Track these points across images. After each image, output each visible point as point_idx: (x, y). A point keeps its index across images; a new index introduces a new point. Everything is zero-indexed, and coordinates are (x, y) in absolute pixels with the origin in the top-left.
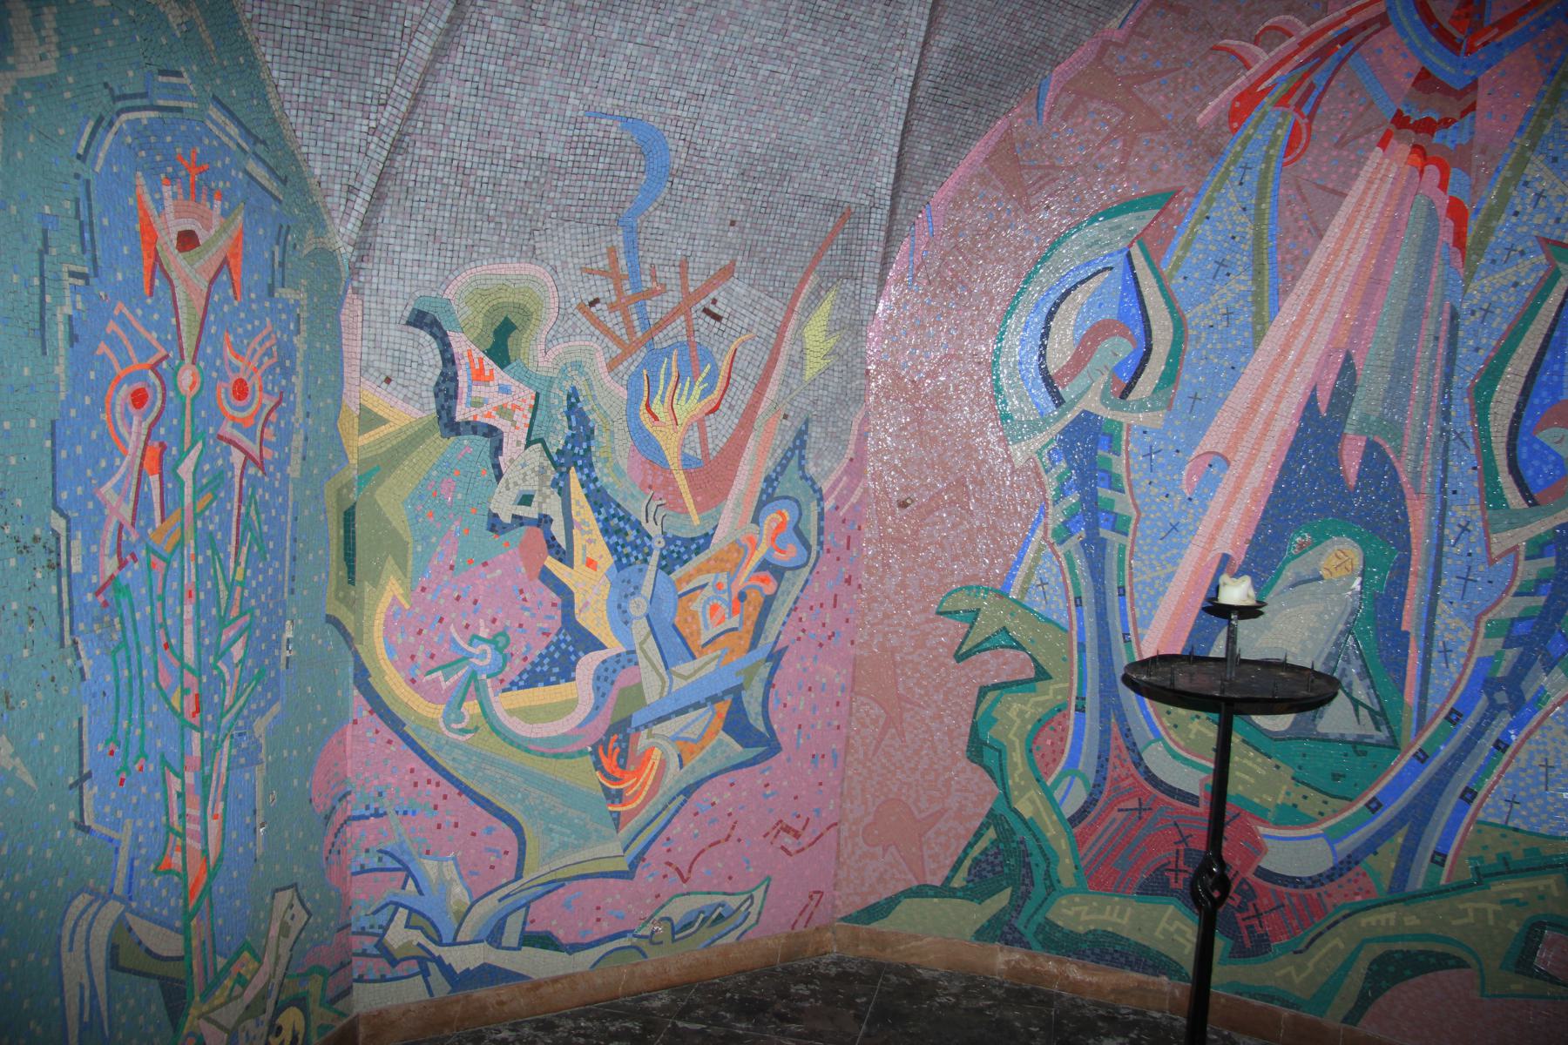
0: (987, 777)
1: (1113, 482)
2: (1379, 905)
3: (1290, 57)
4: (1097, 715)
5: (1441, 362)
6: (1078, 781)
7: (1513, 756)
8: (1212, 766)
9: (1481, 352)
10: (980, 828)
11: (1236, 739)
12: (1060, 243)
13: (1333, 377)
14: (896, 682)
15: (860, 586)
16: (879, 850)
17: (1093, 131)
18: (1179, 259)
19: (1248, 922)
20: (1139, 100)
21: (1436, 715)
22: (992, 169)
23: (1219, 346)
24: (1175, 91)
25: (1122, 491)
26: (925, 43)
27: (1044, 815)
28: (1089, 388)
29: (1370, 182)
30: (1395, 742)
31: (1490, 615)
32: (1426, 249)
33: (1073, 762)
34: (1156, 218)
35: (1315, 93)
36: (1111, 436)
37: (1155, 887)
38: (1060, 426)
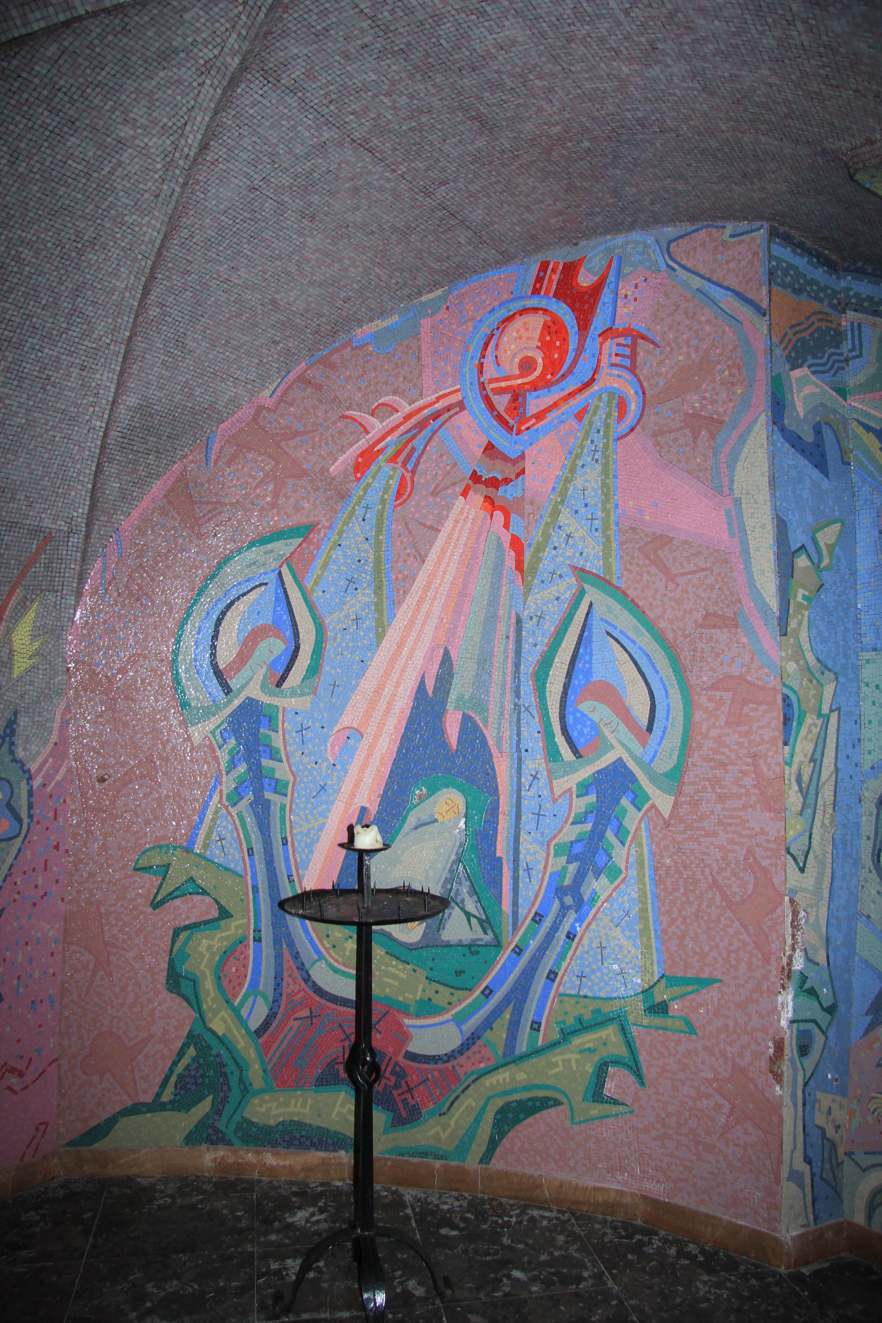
0: (185, 1004)
1: (273, 754)
2: (498, 1068)
4: (272, 943)
5: (512, 655)
6: (260, 1000)
7: (579, 943)
8: (354, 972)
9: (538, 647)
10: (182, 1048)
11: (378, 952)
12: (225, 564)
13: (436, 667)
14: (103, 932)
15: (67, 851)
16: (96, 1078)
17: (250, 476)
18: (319, 577)
19: (403, 1097)
20: (287, 453)
21: (526, 918)
22: (170, 502)
23: (351, 645)
24: (313, 447)
25: (281, 761)
26: (114, 402)
27: (234, 1030)
28: (251, 679)
29: (457, 522)
30: (498, 941)
31: (556, 840)
32: (497, 573)
33: (255, 984)
34: (300, 545)
35: (416, 455)
36: (270, 717)
37: (326, 1080)
38: (229, 710)
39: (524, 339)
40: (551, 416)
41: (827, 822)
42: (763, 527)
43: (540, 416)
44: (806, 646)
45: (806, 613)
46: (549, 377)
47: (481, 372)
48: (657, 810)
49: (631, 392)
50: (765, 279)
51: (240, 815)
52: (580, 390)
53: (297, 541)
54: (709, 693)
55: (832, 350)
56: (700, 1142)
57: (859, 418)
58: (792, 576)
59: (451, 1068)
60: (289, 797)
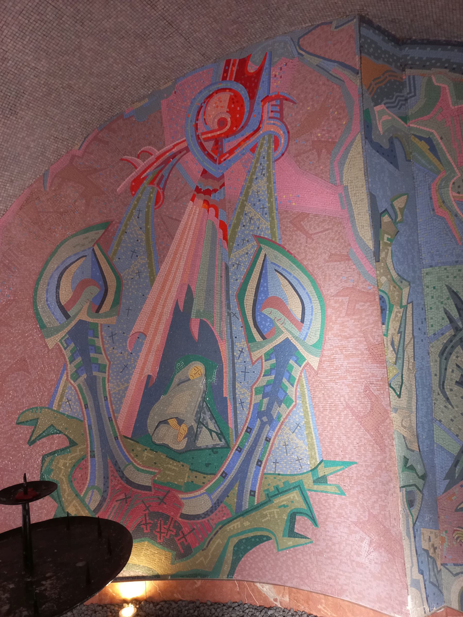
1: (97, 350)
2: (233, 520)
3: (153, 163)
5: (224, 286)
9: (238, 281)
31: (256, 386)
35: (164, 179)
38: (69, 328)
39: (219, 108)
40: (237, 152)
41: (411, 367)
42: (362, 200)
43: (231, 152)
44: (391, 267)
45: (390, 248)
46: (235, 129)
47: (197, 129)
48: (310, 365)
49: (281, 133)
50: (357, 51)
51: (79, 386)
52: (252, 135)
53: (101, 232)
54: (335, 299)
55: (398, 94)
56: (354, 561)
57: (415, 133)
58: (381, 227)
59: (207, 522)
60: (107, 373)
